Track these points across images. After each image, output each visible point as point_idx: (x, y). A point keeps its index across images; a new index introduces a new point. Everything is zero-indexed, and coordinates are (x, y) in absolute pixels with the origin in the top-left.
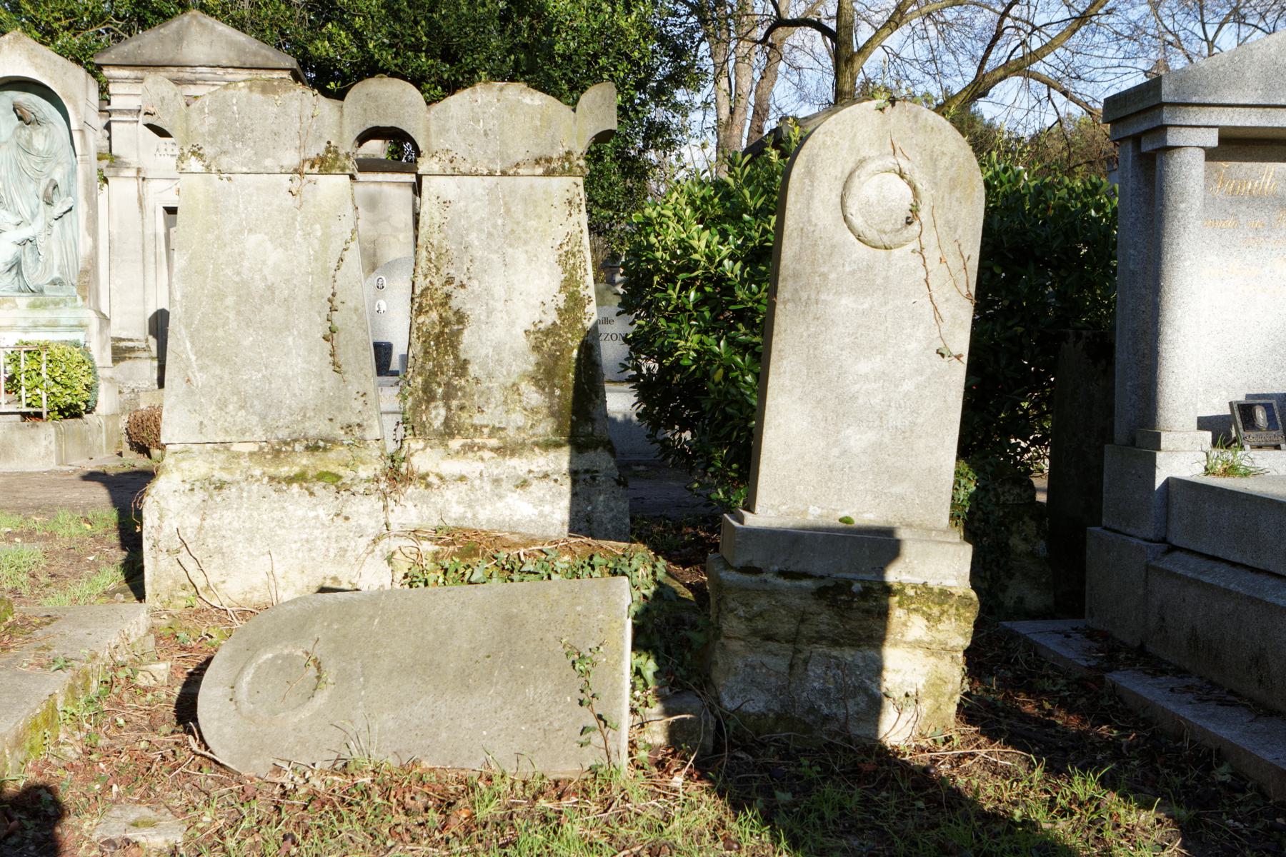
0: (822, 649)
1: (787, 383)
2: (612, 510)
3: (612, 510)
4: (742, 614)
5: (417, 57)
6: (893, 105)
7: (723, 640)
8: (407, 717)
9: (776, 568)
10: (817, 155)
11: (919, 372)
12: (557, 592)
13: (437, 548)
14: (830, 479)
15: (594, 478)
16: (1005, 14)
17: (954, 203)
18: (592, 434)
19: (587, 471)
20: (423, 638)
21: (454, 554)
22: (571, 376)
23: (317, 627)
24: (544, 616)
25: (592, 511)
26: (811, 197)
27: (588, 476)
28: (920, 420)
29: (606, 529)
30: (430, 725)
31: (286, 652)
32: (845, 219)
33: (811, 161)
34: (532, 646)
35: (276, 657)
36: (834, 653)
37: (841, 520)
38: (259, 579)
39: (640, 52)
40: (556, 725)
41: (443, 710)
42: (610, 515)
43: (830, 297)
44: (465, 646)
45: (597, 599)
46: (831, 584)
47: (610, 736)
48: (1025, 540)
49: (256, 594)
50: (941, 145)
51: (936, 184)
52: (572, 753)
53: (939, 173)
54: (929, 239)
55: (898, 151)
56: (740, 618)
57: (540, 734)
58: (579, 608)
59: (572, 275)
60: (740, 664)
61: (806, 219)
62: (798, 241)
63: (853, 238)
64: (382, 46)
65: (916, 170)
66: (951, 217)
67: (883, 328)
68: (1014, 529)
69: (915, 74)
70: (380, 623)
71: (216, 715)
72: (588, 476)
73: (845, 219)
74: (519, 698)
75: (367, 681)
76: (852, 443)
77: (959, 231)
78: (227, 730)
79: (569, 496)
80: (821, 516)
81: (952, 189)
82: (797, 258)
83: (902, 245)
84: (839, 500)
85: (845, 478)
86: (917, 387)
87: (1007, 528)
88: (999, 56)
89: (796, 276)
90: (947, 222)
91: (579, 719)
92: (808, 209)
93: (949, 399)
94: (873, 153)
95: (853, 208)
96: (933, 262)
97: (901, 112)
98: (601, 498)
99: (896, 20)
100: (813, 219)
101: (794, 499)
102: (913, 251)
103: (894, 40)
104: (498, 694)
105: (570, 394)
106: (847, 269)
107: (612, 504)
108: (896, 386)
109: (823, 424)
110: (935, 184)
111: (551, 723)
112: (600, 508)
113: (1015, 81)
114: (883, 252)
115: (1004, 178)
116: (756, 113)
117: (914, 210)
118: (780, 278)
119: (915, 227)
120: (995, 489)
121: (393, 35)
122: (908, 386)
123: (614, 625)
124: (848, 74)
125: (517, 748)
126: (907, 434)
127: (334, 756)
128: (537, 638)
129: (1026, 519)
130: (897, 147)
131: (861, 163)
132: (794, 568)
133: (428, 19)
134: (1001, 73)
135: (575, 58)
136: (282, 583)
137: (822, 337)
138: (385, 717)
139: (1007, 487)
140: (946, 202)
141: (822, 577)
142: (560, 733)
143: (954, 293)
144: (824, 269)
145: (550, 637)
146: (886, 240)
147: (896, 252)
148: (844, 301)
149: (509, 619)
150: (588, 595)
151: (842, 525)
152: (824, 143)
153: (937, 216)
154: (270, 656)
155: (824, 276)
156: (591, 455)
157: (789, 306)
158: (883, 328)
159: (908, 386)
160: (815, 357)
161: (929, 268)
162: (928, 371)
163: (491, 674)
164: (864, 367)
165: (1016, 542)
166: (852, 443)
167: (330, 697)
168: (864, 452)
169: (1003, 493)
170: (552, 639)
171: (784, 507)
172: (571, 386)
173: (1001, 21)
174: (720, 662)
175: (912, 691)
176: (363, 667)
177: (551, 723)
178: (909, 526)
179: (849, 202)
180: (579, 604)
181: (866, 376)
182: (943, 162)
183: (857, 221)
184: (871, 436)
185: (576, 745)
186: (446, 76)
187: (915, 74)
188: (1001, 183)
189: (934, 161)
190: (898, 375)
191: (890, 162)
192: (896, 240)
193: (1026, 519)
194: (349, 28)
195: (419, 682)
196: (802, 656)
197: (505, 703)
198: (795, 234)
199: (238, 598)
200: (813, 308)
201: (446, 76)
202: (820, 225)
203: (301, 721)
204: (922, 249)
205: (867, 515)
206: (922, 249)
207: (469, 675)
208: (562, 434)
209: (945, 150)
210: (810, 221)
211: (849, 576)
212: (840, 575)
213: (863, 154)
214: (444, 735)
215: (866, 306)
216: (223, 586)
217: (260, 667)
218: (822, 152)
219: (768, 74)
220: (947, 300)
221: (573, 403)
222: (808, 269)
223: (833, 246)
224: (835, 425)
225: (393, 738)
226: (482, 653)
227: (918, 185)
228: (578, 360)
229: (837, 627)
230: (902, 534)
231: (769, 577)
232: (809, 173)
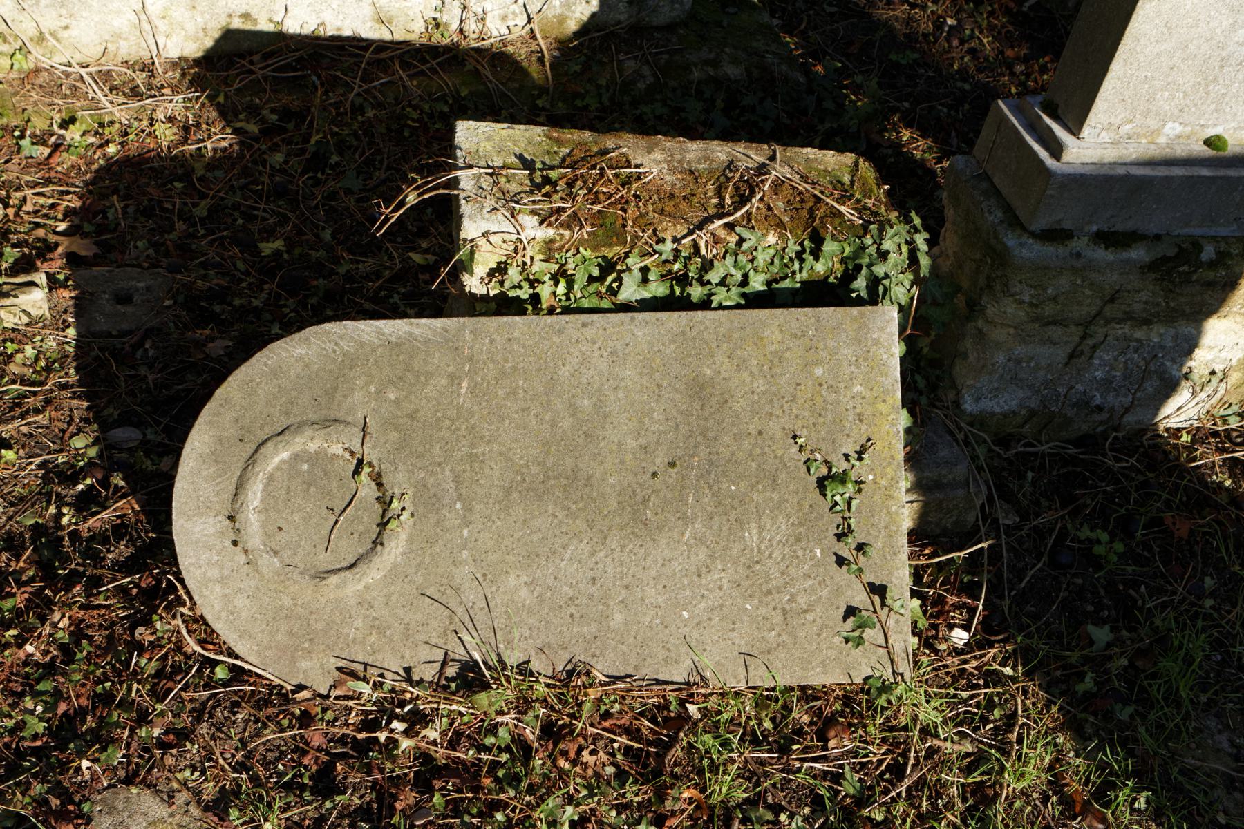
0: (1124, 330)
4: (1027, 298)
7: (980, 323)
8: (551, 581)
9: (1095, 228)
12: (777, 336)
13: (550, 232)
14: (1215, 80)
20: (553, 425)
21: (582, 242)
23: (358, 395)
24: (760, 385)
30: (591, 597)
31: (312, 447)
34: (746, 445)
35: (296, 457)
36: (1139, 334)
37: (1208, 142)
38: (123, 21)
40: (802, 601)
41: (610, 569)
44: (631, 442)
45: (847, 352)
46: (1171, 252)
47: (892, 622)
49: (123, 43)
52: (833, 654)
56: (1021, 302)
57: (778, 618)
58: (818, 371)
60: (1001, 358)
70: (472, 390)
71: (214, 573)
74: (735, 549)
75: (468, 509)
78: (240, 602)
91: (838, 591)
104: (700, 540)
111: (793, 599)
123: (882, 407)
125: (742, 643)
127: (439, 655)
128: (753, 428)
132: (1119, 227)
136: (162, 26)
138: (512, 581)
141: (1157, 237)
142: (810, 617)
145: (774, 427)
149: (699, 389)
150: (832, 343)
151: (1208, 152)
154: (285, 455)
163: (682, 499)
167: (410, 540)
170: (779, 434)
174: (972, 357)
175: (1218, 368)
176: (458, 480)
177: (793, 599)
180: (818, 363)
185: (838, 640)
195: (560, 514)
196: (1090, 342)
197: (712, 557)
199: (91, 52)
203: (367, 587)
207: (645, 501)
211: (1197, 231)
212: (1186, 231)
214: (618, 617)
216: (65, 34)
217: (271, 478)
225: (532, 621)
226: (661, 460)
229: (1158, 304)
231: (1079, 244)
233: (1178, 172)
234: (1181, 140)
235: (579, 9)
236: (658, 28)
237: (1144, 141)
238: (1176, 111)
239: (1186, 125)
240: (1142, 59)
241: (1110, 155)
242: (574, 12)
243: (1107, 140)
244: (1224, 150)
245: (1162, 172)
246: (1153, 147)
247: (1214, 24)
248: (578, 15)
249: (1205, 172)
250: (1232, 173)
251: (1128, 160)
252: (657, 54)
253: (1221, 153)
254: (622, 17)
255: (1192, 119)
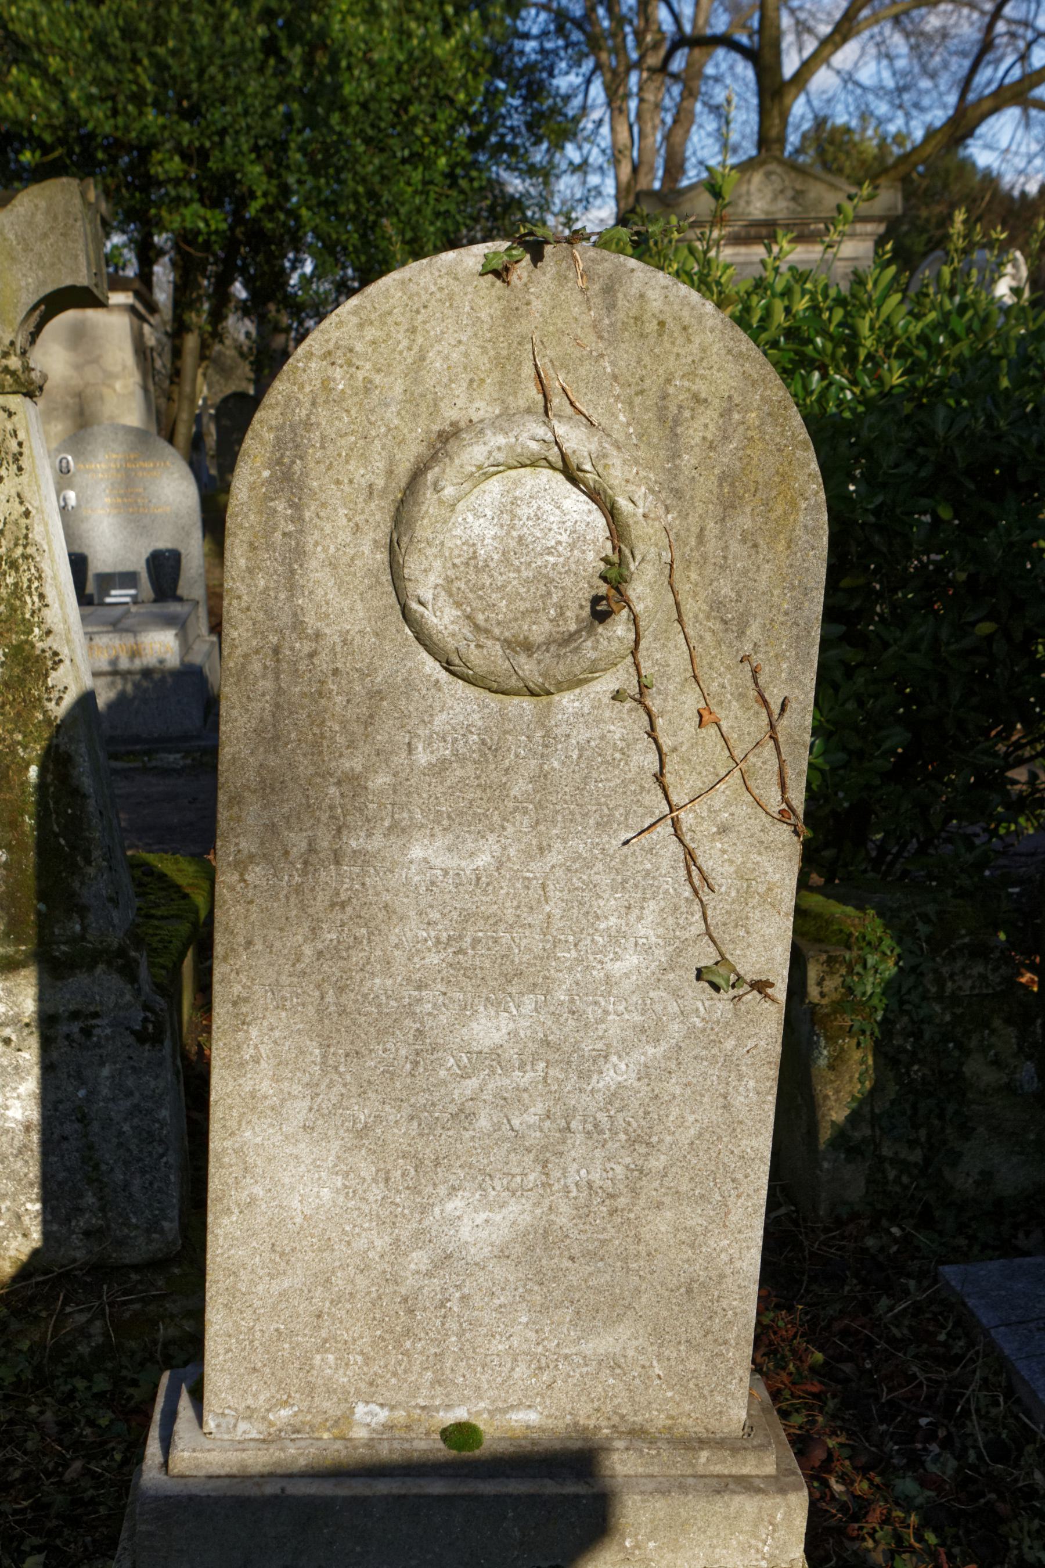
1: (266, 1087)
2: (130, 1094)
3: (130, 1094)
5: (141, 113)
6: (537, 257)
10: (308, 425)
11: (650, 1031)
14: (408, 1332)
15: (87, 1032)
16: (996, 14)
17: (735, 547)
18: (83, 938)
19: (75, 1015)
22: (29, 821)
25: (88, 1099)
26: (299, 553)
27: (75, 1028)
28: (657, 1163)
29: (121, 1133)
32: (406, 614)
33: (291, 443)
39: (468, 94)
42: (126, 1104)
43: (377, 842)
48: (996, 1063)
50: (691, 375)
51: (678, 494)
53: (688, 460)
54: (665, 656)
55: (557, 401)
59: (13, 609)
61: (286, 619)
62: (267, 684)
63: (431, 667)
64: (90, 100)
65: (615, 459)
66: (726, 590)
67: (537, 919)
68: (973, 1043)
69: (882, 108)
72: (75, 1028)
73: (406, 614)
76: (465, 1233)
77: (754, 631)
79: (36, 1071)
80: (388, 1427)
81: (729, 506)
82: (269, 736)
83: (580, 683)
84: (438, 1382)
85: (452, 1325)
86: (644, 1074)
87: (959, 1046)
88: (988, 77)
89: (270, 787)
90: (717, 605)
92: (292, 588)
93: (738, 1101)
94: (482, 409)
95: (426, 582)
96: (678, 728)
97: (561, 279)
98: (106, 1072)
99: (845, 29)
100: (310, 620)
101: (311, 1390)
102: (618, 696)
103: (845, 56)
105: (30, 858)
106: (423, 757)
107: (130, 1083)
108: (584, 1075)
109: (377, 1192)
110: (673, 493)
112: (105, 1092)
113: (1011, 114)
114: (527, 704)
115: (958, 325)
116: (667, 171)
117: (615, 577)
118: (222, 797)
119: (620, 628)
120: (936, 971)
121: (100, 81)
122: (617, 1073)
124: (775, 113)
126: (622, 1202)
129: (997, 1023)
130: (556, 381)
131: (445, 441)
133: (152, 55)
134: (986, 106)
135: (373, 106)
137: (357, 957)
139: (959, 964)
140: (712, 545)
143: (744, 809)
144: (355, 763)
146: (528, 667)
147: (568, 701)
148: (417, 852)
152: (326, 384)
153: (684, 588)
155: (354, 783)
156: (82, 979)
157: (256, 874)
158: (537, 919)
159: (617, 1073)
160: (343, 1012)
161: (666, 742)
162: (675, 1029)
164: (488, 1029)
165: (977, 1069)
166: (465, 1233)
168: (502, 1254)
169: (952, 976)
171: (285, 1413)
172: (30, 841)
173: (991, 26)
178: (637, 1434)
179: (412, 567)
181: (495, 1053)
182: (700, 428)
183: (442, 619)
184: (517, 1214)
186: (185, 141)
187: (882, 108)
188: (954, 338)
189: (670, 424)
190: (587, 1047)
191: (531, 434)
192: (560, 671)
193: (997, 1023)
194: (39, 69)
198: (256, 667)
200: (327, 875)
201: (185, 141)
202: (332, 635)
204: (643, 687)
205: (517, 1410)
206: (643, 687)
208: (19, 941)
209: (702, 388)
210: (298, 625)
213: (451, 414)
215: (483, 860)
218: (322, 414)
219: (683, 119)
220: (724, 830)
221: (39, 877)
222: (305, 767)
223: (376, 695)
224: (415, 1190)
227: (622, 502)
228: (42, 786)
230: (622, 1464)
232: (287, 481)
233: (383, 1487)
234: (397, 1433)
235: (14, 1244)
236: (136, 1268)
237: (326, 1436)
238: (363, 1385)
239: (392, 1408)
240: (257, 1303)
241: (258, 1460)
242: (6, 1249)
243: (254, 1435)
244: (479, 1443)
245: (359, 1488)
246: (339, 1445)
247: (360, 1244)
248: (12, 1253)
249: (437, 1487)
250: (488, 1488)
251: (295, 1469)
252: (124, 1303)
253: (465, 1454)
254: (78, 1254)
255: (400, 1397)
